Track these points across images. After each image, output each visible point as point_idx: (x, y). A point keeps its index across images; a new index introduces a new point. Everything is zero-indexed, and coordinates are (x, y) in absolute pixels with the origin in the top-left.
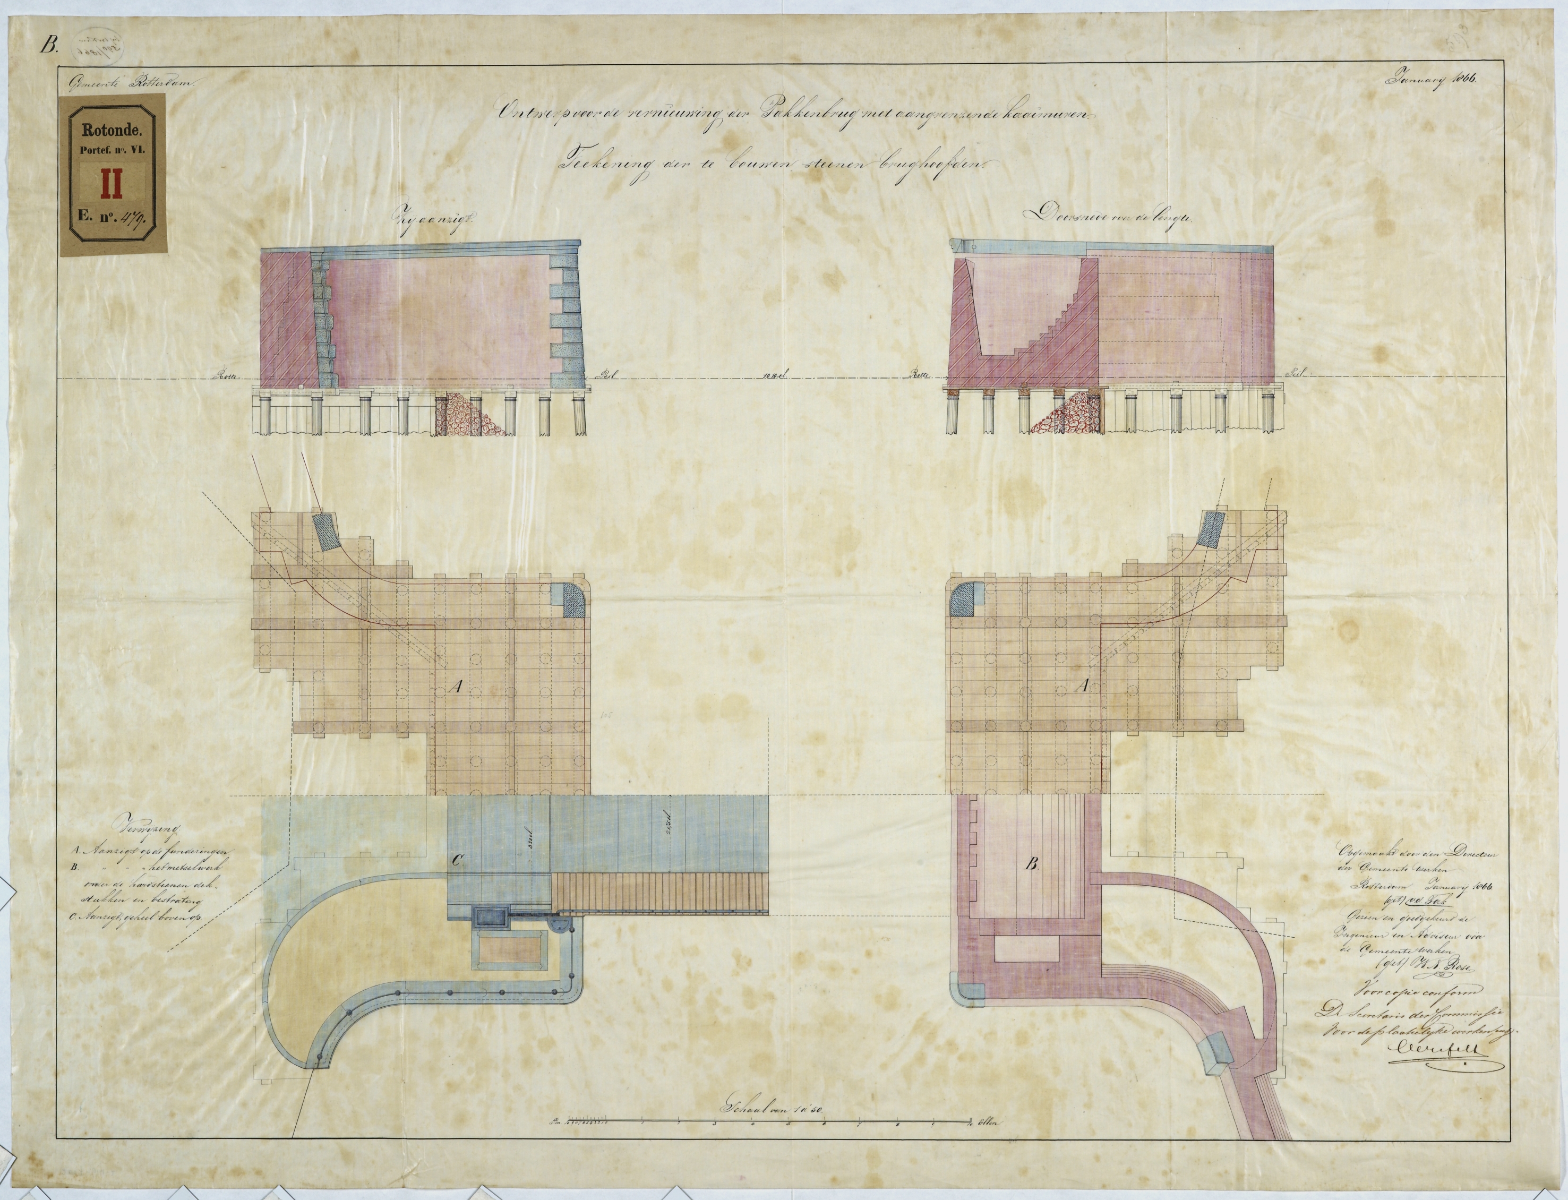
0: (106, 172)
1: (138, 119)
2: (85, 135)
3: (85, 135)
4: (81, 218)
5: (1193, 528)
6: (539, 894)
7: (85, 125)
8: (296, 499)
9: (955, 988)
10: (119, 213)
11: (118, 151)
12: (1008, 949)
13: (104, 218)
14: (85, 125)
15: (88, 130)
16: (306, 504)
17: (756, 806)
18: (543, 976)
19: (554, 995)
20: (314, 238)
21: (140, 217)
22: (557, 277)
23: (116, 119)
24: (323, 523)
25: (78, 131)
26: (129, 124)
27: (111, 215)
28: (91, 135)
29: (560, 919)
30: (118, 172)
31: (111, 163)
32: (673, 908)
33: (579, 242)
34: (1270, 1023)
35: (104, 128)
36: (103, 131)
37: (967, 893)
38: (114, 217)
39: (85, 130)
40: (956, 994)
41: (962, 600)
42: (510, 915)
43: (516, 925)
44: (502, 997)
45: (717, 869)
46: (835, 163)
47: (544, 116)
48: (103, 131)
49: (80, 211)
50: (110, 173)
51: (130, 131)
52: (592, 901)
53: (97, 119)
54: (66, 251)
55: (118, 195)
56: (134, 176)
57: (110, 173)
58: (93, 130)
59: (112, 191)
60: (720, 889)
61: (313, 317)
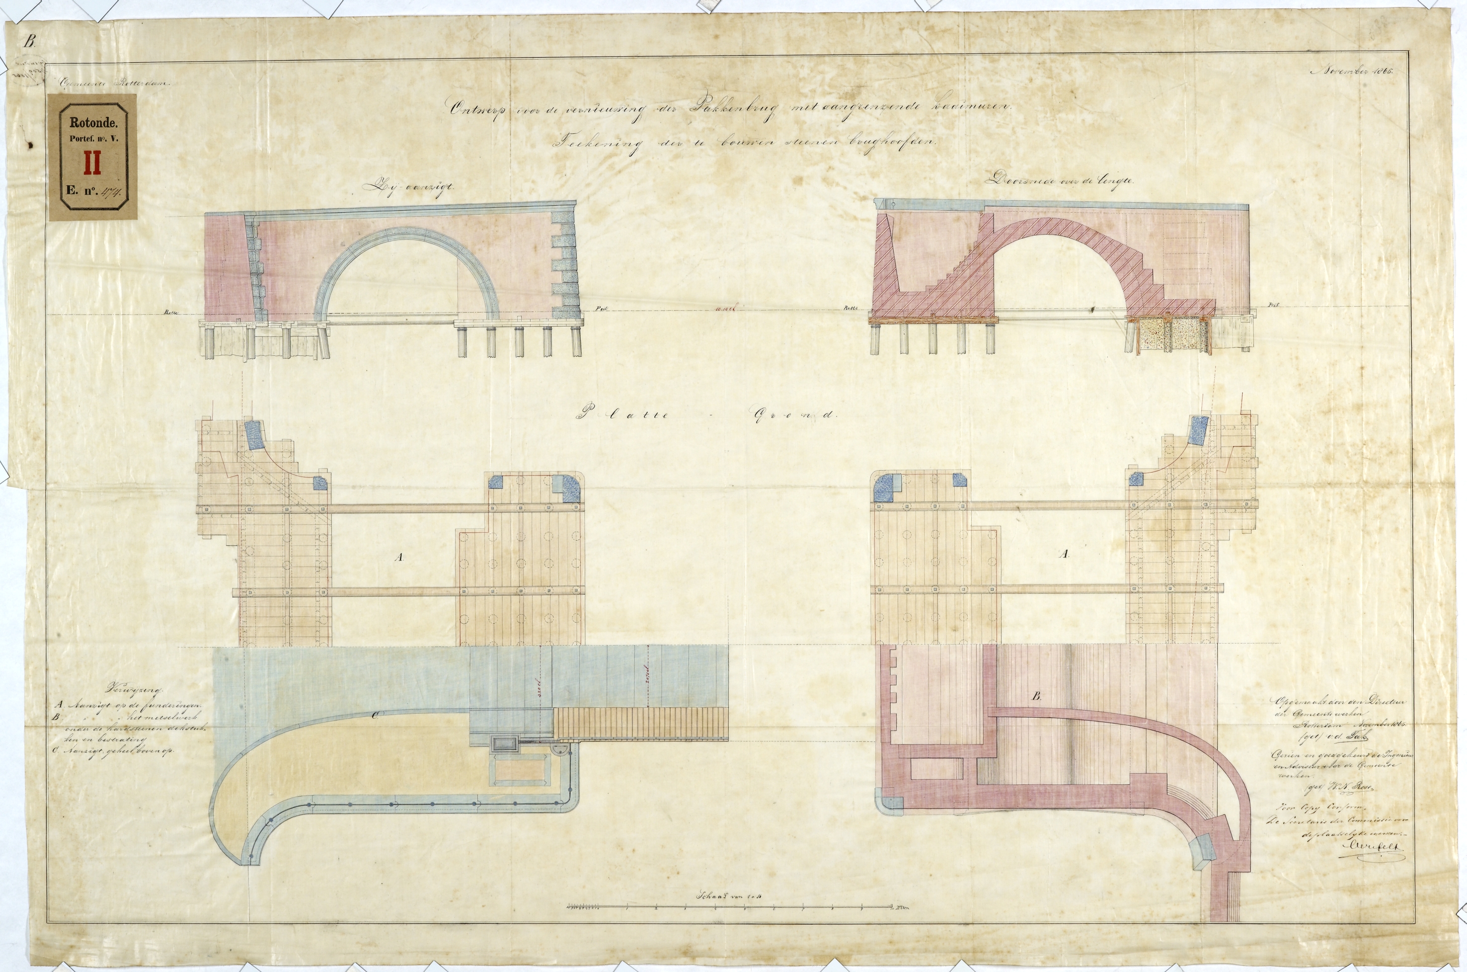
0: (87, 153)
1: (117, 116)
2: (72, 126)
3: (72, 126)
4: (69, 192)
5: (1183, 430)
6: (541, 725)
7: (72, 118)
8: (230, 413)
9: (879, 800)
10: (99, 189)
11: (100, 139)
12: (922, 769)
13: (88, 192)
14: (72, 118)
15: (74, 123)
16: (237, 415)
17: (719, 656)
18: (549, 790)
19: (556, 805)
20: (81, 226)
21: (117, 193)
22: (557, 229)
23: (95, 114)
24: (253, 432)
25: (66, 123)
26: (108, 118)
27: (94, 189)
28: (77, 126)
29: (565, 747)
30: (97, 153)
31: (92, 146)
32: (684, 736)
33: (574, 203)
34: (1247, 833)
35: (87, 121)
36: (86, 123)
37: (886, 724)
38: (95, 191)
39: (72, 122)
40: (882, 807)
41: (885, 489)
42: (520, 742)
43: (524, 749)
44: (351, 808)
45: (683, 706)
46: (811, 141)
47: (486, 112)
48: (86, 123)
49: (68, 187)
50: (91, 156)
51: (109, 123)
52: (571, 731)
53: (81, 114)
54: (54, 216)
55: (97, 172)
56: (112, 158)
57: (91, 156)
58: (78, 123)
59: (92, 168)
60: (678, 721)
61: (251, 272)
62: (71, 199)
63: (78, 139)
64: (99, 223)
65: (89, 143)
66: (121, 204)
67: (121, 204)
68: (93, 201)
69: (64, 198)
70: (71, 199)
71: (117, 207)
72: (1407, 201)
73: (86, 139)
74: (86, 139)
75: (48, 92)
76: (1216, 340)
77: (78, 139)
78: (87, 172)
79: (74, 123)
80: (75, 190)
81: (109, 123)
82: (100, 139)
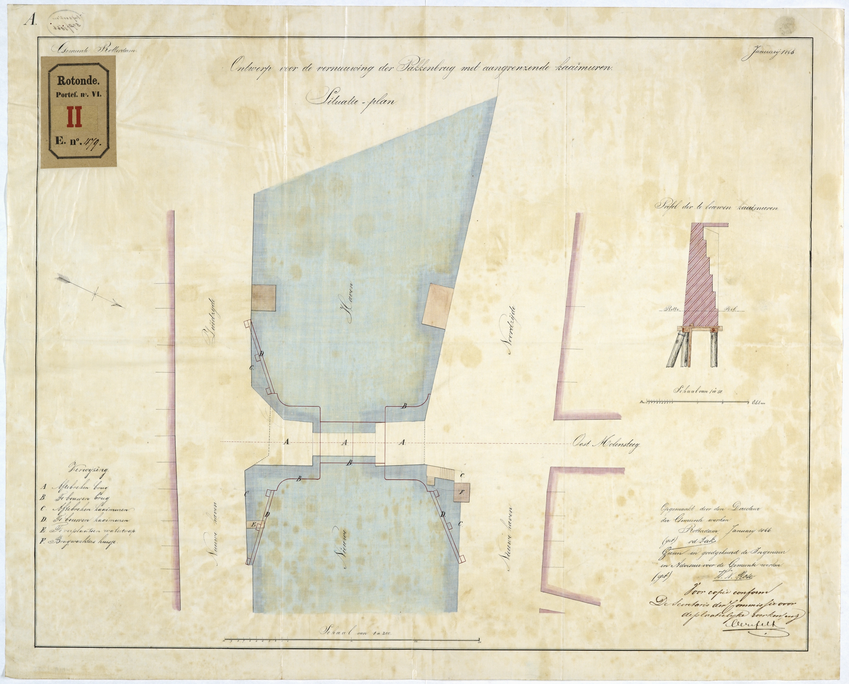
0: (70, 109)
2: (60, 84)
3: (60, 84)
4: (57, 143)
7: (59, 77)
11: (83, 95)
14: (59, 77)
23: (80, 73)
25: (55, 81)
26: (90, 76)
27: (78, 140)
28: (64, 84)
30: (79, 108)
31: (74, 102)
35: (73, 79)
36: (72, 81)
39: (60, 80)
48: (72, 81)
49: (57, 138)
51: (91, 81)
53: (67, 73)
55: (79, 125)
56: (92, 110)
58: (65, 81)
62: (60, 150)
63: (64, 95)
64: (88, 169)
65: (72, 99)
66: (101, 151)
67: (101, 151)
68: (80, 150)
69: (52, 149)
70: (60, 150)
71: (59, 156)
72: (166, 646)
73: (70, 95)
74: (70, 95)
75: (42, 54)
76: (724, 221)
77: (64, 95)
78: (70, 125)
79: (61, 81)
80: (64, 140)
81: (91, 81)
82: (83, 95)
